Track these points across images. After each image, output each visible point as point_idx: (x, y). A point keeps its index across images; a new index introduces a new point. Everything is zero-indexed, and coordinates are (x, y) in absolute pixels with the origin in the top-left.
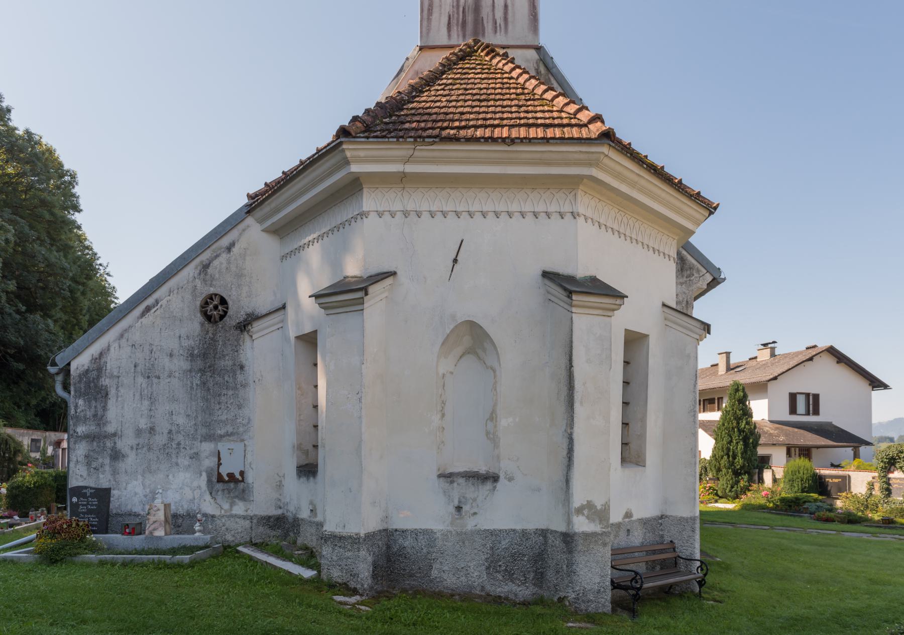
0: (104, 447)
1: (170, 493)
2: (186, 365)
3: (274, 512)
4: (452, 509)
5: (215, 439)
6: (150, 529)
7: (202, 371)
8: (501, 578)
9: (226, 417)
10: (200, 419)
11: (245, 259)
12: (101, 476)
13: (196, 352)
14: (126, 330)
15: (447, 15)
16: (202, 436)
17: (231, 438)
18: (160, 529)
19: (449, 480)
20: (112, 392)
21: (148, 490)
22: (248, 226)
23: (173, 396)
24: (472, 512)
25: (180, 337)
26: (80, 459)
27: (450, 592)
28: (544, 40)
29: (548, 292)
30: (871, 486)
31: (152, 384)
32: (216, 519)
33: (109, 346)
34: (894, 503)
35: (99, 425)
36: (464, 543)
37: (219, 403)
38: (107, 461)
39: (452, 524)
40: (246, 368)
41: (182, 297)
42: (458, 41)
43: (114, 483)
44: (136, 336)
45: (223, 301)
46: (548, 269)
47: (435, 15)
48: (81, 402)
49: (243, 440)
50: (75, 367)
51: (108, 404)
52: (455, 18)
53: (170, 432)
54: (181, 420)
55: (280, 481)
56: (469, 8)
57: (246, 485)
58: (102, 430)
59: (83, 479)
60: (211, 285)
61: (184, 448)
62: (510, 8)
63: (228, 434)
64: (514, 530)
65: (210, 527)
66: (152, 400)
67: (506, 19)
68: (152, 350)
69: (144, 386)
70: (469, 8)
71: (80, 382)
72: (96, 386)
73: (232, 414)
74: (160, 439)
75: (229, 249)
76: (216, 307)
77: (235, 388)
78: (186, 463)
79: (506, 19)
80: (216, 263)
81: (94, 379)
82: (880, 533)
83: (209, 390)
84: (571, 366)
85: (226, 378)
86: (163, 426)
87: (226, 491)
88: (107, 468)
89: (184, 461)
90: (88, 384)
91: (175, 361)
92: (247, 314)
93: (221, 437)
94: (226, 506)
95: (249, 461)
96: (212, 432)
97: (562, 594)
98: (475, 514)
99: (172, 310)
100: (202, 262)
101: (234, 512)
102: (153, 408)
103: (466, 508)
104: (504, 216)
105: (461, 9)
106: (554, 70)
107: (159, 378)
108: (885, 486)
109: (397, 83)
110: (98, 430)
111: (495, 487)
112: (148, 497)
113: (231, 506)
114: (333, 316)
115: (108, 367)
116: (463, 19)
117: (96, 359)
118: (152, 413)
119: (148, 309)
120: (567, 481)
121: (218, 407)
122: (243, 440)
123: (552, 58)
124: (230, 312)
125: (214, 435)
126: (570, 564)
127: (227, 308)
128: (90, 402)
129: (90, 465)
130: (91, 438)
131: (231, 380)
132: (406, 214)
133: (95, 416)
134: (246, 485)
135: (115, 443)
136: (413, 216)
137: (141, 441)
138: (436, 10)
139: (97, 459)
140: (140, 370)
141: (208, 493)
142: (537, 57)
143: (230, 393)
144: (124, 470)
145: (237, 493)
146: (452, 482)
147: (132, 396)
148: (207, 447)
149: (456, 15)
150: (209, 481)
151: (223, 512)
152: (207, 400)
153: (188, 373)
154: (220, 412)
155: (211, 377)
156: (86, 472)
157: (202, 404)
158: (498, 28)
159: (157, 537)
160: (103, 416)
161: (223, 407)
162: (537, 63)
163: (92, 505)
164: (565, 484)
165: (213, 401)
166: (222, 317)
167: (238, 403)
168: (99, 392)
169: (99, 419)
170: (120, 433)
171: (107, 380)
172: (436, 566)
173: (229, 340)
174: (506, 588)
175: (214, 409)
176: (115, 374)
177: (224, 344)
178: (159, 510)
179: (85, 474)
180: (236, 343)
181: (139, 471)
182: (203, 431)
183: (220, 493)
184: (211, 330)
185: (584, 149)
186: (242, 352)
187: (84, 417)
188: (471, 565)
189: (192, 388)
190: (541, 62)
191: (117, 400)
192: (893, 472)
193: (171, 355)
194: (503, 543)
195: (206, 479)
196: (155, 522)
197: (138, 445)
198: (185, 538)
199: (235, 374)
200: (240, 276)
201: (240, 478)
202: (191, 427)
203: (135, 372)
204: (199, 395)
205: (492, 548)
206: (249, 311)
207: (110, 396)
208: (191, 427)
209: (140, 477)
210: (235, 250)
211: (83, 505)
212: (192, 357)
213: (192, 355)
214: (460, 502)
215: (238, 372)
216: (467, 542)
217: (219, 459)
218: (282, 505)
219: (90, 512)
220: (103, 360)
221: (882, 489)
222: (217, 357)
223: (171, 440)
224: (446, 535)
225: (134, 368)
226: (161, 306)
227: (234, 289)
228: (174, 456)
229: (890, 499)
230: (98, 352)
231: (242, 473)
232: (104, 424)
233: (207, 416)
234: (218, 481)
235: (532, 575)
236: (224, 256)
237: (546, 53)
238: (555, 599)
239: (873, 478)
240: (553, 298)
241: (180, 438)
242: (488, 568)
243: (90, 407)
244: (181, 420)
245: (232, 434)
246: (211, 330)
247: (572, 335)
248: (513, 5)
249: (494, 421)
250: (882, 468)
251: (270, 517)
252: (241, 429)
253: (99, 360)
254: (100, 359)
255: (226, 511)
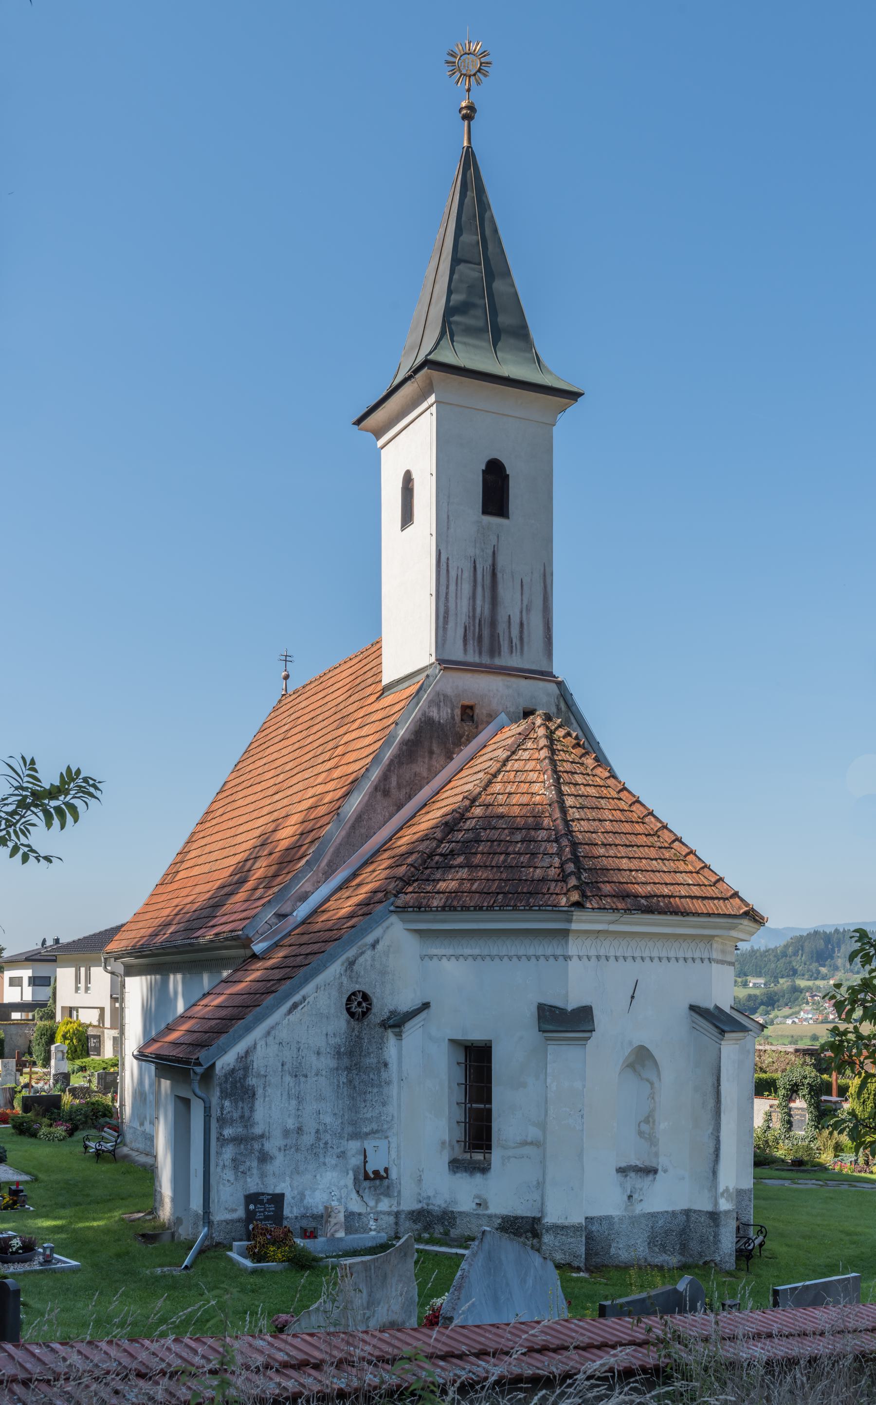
0: (251, 1150)
1: (317, 1193)
2: (332, 1063)
3: (417, 1206)
4: (626, 1198)
5: (361, 1138)
6: (332, 1231)
7: (348, 1069)
8: (657, 1250)
9: (371, 1114)
10: (346, 1117)
11: (388, 957)
12: (249, 1180)
13: (342, 1050)
14: (273, 1028)
15: (463, 625)
16: (349, 1134)
17: (376, 1136)
18: (341, 1230)
19: (624, 1174)
20: (260, 1092)
21: (296, 1192)
22: (392, 924)
23: (320, 1095)
24: (639, 1199)
25: (327, 1035)
26: (227, 1163)
27: (624, 1265)
28: (559, 670)
29: (693, 1022)
30: (769, 1117)
31: (300, 1084)
32: (362, 1217)
33: (255, 1044)
34: (796, 1139)
35: (246, 1126)
36: (634, 1224)
37: (365, 1101)
38: (255, 1164)
39: (626, 1209)
40: (390, 1066)
41: (329, 994)
42: (474, 657)
43: (262, 1186)
44: (283, 1034)
45: (366, 997)
46: (693, 1004)
47: (451, 625)
48: (227, 1103)
49: (387, 1137)
50: (221, 1067)
51: (256, 1105)
52: (471, 631)
53: (317, 1132)
54: (328, 1119)
55: (420, 1176)
56: (485, 621)
57: (390, 1181)
58: (250, 1131)
59: (230, 1184)
60: (357, 982)
61: (331, 1147)
62: (525, 627)
63: (373, 1132)
64: (667, 1212)
65: (357, 1225)
66: (300, 1099)
67: (521, 639)
68: (299, 1048)
69: (292, 1085)
70: (485, 621)
71: (226, 1082)
72: (242, 1086)
73: (377, 1111)
74: (308, 1139)
75: (374, 946)
76: (359, 1004)
77: (380, 1086)
78: (333, 1162)
79: (521, 639)
80: (361, 960)
81: (240, 1078)
82: (798, 1179)
83: (355, 1088)
84: (719, 1084)
85: (371, 1076)
86: (311, 1126)
87: (372, 1189)
88: (255, 1171)
89: (331, 1160)
90: (234, 1084)
91: (322, 1059)
92: (390, 1012)
93: (367, 1134)
94: (372, 1203)
95: (393, 1158)
96: (358, 1130)
97: (708, 1259)
98: (641, 1200)
99: (318, 1007)
100: (348, 959)
101: (379, 1209)
102: (301, 1108)
103: (635, 1196)
104: (665, 961)
105: (477, 621)
106: (573, 708)
107: (306, 1076)
108: (787, 1118)
109: (418, 704)
110: (245, 1132)
111: (655, 1178)
112: (296, 1199)
113: (377, 1203)
114: (555, 1046)
115: (255, 1066)
116: (479, 632)
117: (242, 1057)
118: (300, 1113)
119: (295, 1006)
120: (715, 1173)
121: (363, 1105)
122: (387, 1137)
123: (571, 694)
124: (375, 1009)
125: (360, 1133)
126: (716, 1235)
127: (370, 1004)
128: (236, 1103)
129: (237, 1169)
130: (237, 1140)
131: (376, 1078)
132: (598, 957)
133: (242, 1117)
134: (390, 1181)
135: (263, 1145)
136: (603, 959)
137: (289, 1142)
138: (451, 619)
139: (245, 1162)
140: (287, 1069)
141: (354, 1191)
142: (558, 692)
143: (375, 1090)
144: (272, 1172)
145: (382, 1190)
146: (626, 1176)
147: (279, 1095)
148: (354, 1146)
149: (472, 628)
150: (356, 1179)
151: (368, 1209)
152: (353, 1098)
153: (335, 1071)
154: (365, 1110)
155: (357, 1074)
156: (234, 1176)
157: (348, 1102)
158: (514, 648)
159: (338, 1238)
160: (249, 1118)
161: (368, 1105)
162: (557, 698)
163: (269, 1211)
164: (711, 1174)
165: (358, 1099)
166: (364, 1014)
167: (382, 1100)
168: (246, 1092)
169: (247, 1121)
170: (267, 1134)
171: (254, 1080)
172: (614, 1245)
173: (374, 1037)
174: (661, 1259)
175: (359, 1107)
176: (262, 1073)
177: (370, 1042)
178: (339, 1212)
179: (232, 1179)
180: (380, 1041)
181: (287, 1173)
182: (349, 1129)
183: (367, 1190)
184: (357, 1027)
185: (730, 920)
186: (386, 1049)
187: (230, 1119)
188: (638, 1241)
189: (338, 1086)
190: (562, 698)
191: (264, 1100)
192: (794, 1101)
193: (318, 1053)
194: (660, 1222)
195: (353, 1178)
196: (335, 1224)
197: (286, 1146)
198: (364, 1238)
199: (379, 1072)
200: (383, 973)
201: (385, 1175)
202: (338, 1126)
203: (282, 1071)
204: (345, 1093)
205: (652, 1227)
206: (392, 1008)
207: (257, 1096)
208: (338, 1126)
209: (287, 1178)
210: (379, 947)
211: (260, 1212)
212: (338, 1054)
213: (338, 1053)
214: (631, 1192)
215: (383, 1069)
216: (635, 1224)
217: (365, 1157)
218: (421, 1199)
219: (267, 1218)
220: (249, 1059)
221: (782, 1120)
222: (363, 1053)
223: (318, 1139)
224: (621, 1219)
225: (281, 1067)
226: (309, 1002)
227: (378, 986)
228: (321, 1156)
229: (792, 1133)
230: (244, 1050)
231: (386, 1170)
232: (252, 1126)
233: (353, 1114)
234: (365, 1179)
235: (677, 1247)
236: (369, 953)
237: (566, 689)
238: (701, 1263)
239: (771, 1106)
240: (698, 1027)
241: (327, 1137)
242: (649, 1244)
243: (237, 1107)
244: (328, 1119)
245: (377, 1132)
246: (357, 1027)
247: (720, 1061)
248: (528, 624)
249: (651, 1124)
250: (784, 1096)
251: (413, 1212)
252: (385, 1126)
253: (245, 1058)
254: (246, 1057)
255: (371, 1208)
